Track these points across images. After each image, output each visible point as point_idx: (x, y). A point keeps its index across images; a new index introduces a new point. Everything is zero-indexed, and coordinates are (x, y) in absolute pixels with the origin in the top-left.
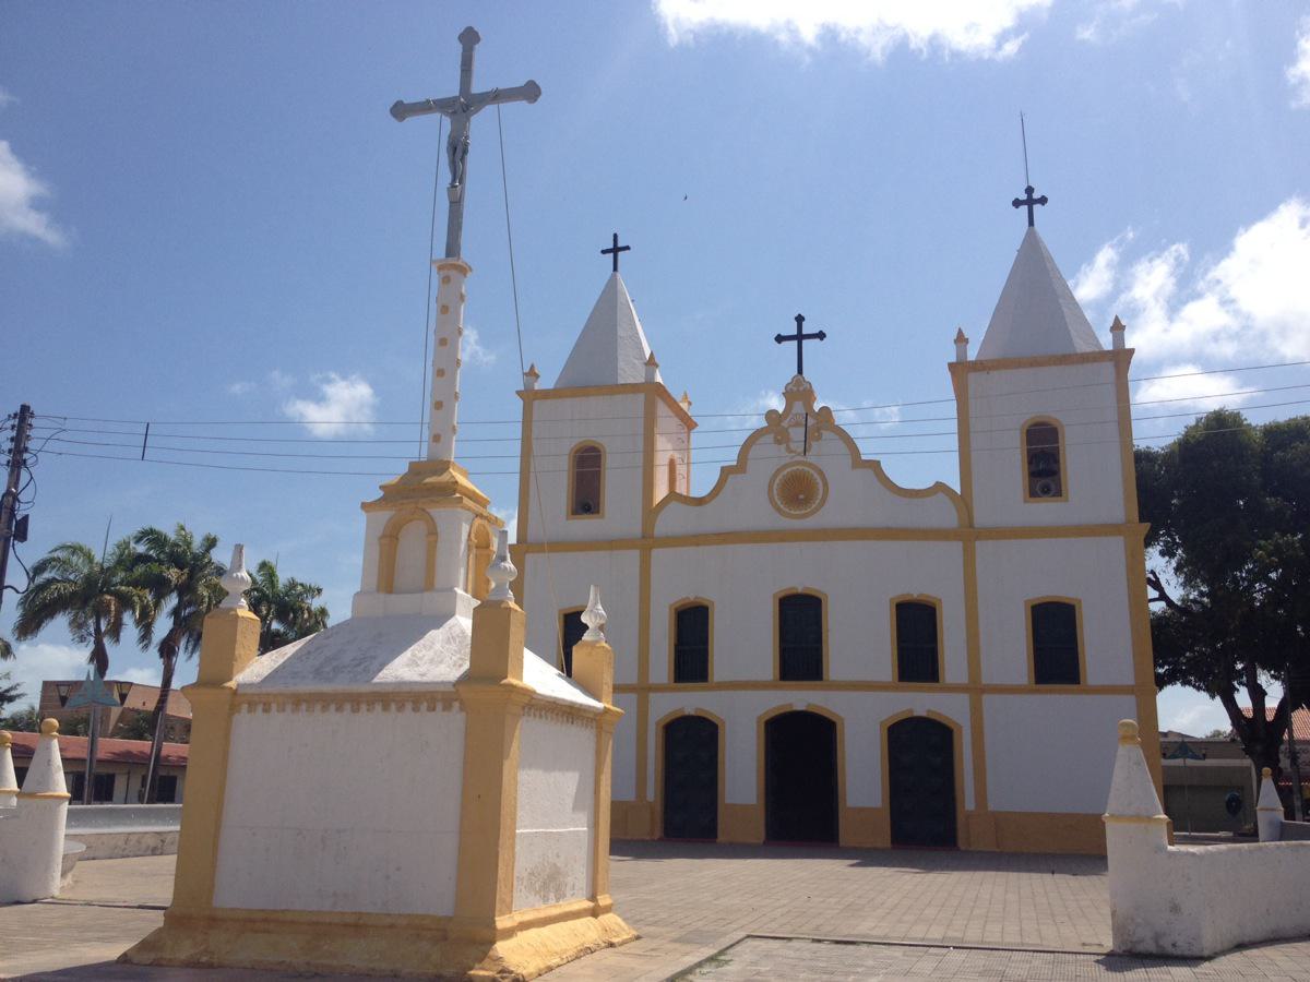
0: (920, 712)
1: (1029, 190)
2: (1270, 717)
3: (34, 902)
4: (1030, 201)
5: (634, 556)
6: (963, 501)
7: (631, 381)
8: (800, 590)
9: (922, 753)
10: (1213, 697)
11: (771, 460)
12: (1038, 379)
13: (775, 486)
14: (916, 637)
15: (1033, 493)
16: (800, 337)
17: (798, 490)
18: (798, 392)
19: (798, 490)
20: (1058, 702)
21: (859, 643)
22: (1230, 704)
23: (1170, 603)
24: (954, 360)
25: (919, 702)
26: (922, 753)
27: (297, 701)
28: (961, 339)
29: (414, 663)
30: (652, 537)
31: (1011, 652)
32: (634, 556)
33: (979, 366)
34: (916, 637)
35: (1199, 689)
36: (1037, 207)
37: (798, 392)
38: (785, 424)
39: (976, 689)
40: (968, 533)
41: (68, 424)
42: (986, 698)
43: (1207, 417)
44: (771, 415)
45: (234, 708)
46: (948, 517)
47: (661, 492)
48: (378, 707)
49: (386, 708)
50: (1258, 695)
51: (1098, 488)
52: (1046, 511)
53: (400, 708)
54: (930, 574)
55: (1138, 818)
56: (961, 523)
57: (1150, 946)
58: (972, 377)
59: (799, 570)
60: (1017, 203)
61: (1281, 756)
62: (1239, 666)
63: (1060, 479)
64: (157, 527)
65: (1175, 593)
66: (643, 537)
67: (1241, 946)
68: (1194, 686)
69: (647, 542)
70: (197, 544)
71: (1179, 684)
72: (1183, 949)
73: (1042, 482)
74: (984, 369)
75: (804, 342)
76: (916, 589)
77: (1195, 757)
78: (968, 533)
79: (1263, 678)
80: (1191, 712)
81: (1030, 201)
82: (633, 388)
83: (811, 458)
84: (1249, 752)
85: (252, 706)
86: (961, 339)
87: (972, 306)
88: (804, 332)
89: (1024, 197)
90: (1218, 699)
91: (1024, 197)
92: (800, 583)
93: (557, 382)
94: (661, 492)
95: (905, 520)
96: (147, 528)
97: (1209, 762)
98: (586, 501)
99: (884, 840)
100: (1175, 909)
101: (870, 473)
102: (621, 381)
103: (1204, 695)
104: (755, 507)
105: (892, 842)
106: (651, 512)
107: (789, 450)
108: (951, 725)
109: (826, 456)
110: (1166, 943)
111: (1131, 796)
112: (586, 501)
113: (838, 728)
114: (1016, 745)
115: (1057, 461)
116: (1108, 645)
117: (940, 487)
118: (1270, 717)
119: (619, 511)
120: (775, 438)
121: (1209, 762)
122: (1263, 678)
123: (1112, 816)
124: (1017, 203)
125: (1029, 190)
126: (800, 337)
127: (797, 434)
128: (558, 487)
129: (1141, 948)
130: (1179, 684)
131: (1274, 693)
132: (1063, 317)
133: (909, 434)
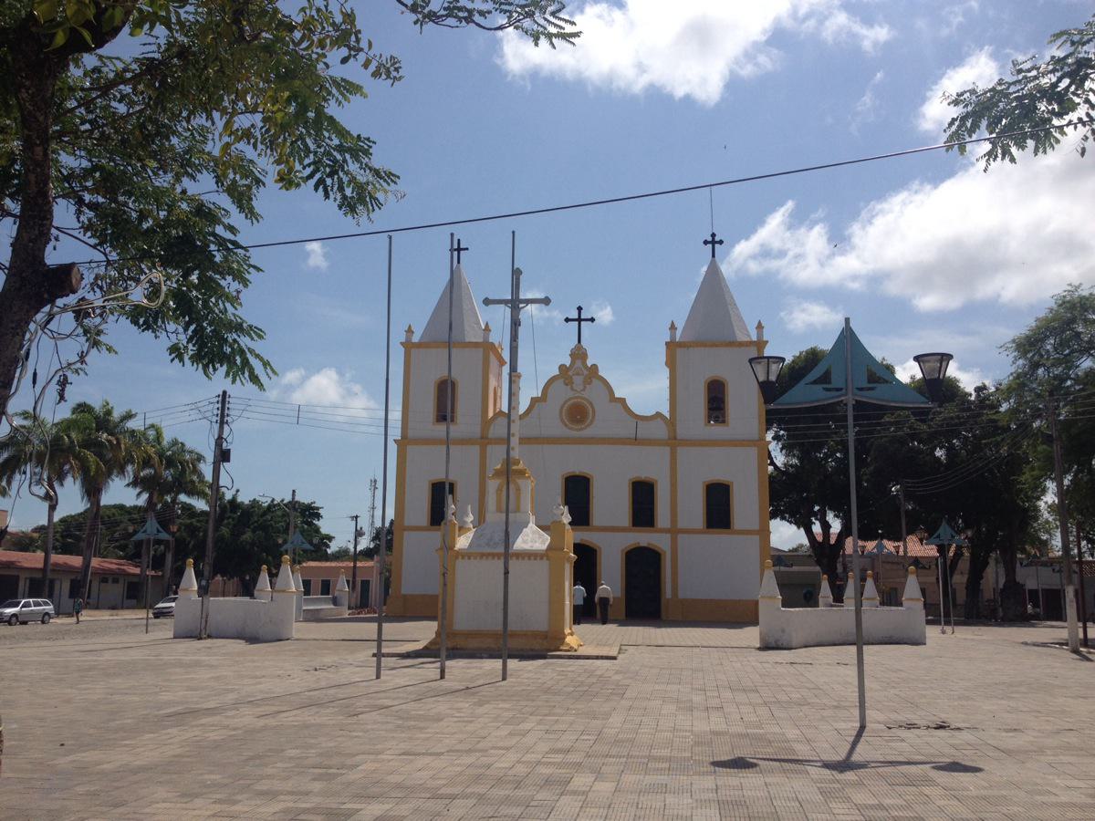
0: (644, 544)
1: (713, 235)
2: (832, 541)
3: (288, 640)
4: (713, 242)
5: (476, 449)
6: (671, 423)
7: (474, 340)
8: (577, 473)
9: (643, 566)
10: (799, 528)
11: (562, 394)
12: (709, 330)
13: (564, 411)
14: (643, 499)
15: (709, 418)
16: (579, 320)
17: (578, 414)
18: (579, 354)
19: (578, 414)
20: (719, 539)
21: (611, 504)
22: (809, 533)
23: (776, 467)
24: (669, 340)
25: (643, 538)
26: (643, 566)
27: (482, 555)
28: (673, 327)
29: (524, 542)
30: (487, 438)
31: (694, 509)
32: (476, 449)
33: (681, 345)
34: (643, 499)
35: (791, 522)
36: (716, 245)
37: (579, 354)
38: (570, 373)
39: (674, 531)
40: (674, 442)
41: (250, 403)
42: (680, 536)
43: (806, 352)
44: (562, 367)
45: (457, 558)
46: (661, 431)
47: (491, 414)
48: (496, 558)
49: (529, 559)
50: (826, 527)
51: (745, 404)
52: (716, 431)
53: (523, 558)
54: (651, 465)
55: (770, 598)
56: (668, 433)
57: (774, 645)
58: (679, 352)
59: (577, 461)
60: (706, 242)
61: (838, 565)
62: (817, 508)
63: (724, 413)
64: (88, 402)
65: (780, 459)
66: (482, 438)
67: (806, 647)
68: (788, 521)
69: (484, 441)
70: (116, 415)
71: (778, 519)
72: (785, 645)
73: (716, 413)
74: (684, 347)
75: (582, 323)
76: (644, 475)
77: (786, 566)
78: (674, 442)
79: (830, 517)
80: (786, 535)
81: (713, 242)
82: (476, 345)
83: (585, 394)
84: (818, 563)
85: (463, 558)
86: (673, 327)
87: (679, 307)
88: (582, 317)
89: (710, 239)
90: (802, 529)
91: (710, 239)
92: (577, 469)
93: (422, 337)
94: (491, 414)
95: (637, 432)
96: (74, 406)
97: (795, 568)
98: (444, 413)
99: (624, 617)
100: (783, 631)
101: (619, 405)
102: (467, 340)
103: (794, 527)
104: (552, 423)
105: (626, 616)
106: (486, 423)
107: (572, 389)
108: (660, 551)
109: (593, 394)
110: (780, 644)
111: (768, 592)
112: (444, 413)
113: (598, 553)
114: (696, 561)
115: (723, 402)
116: (747, 501)
117: (658, 415)
118: (832, 541)
119: (466, 421)
120: (564, 382)
121: (795, 568)
122: (830, 517)
123: (762, 597)
124: (706, 242)
125: (713, 235)
126: (579, 320)
127: (578, 380)
128: (428, 405)
129: (770, 646)
130: (778, 519)
131: (836, 526)
132: (730, 317)
133: (644, 387)
